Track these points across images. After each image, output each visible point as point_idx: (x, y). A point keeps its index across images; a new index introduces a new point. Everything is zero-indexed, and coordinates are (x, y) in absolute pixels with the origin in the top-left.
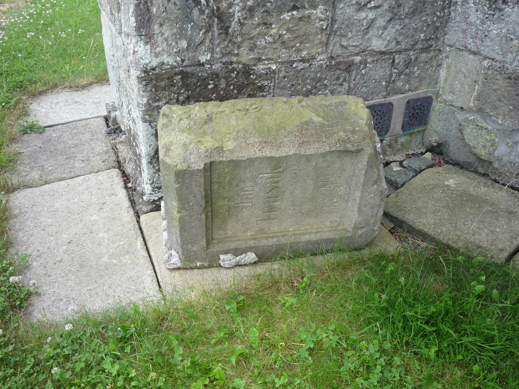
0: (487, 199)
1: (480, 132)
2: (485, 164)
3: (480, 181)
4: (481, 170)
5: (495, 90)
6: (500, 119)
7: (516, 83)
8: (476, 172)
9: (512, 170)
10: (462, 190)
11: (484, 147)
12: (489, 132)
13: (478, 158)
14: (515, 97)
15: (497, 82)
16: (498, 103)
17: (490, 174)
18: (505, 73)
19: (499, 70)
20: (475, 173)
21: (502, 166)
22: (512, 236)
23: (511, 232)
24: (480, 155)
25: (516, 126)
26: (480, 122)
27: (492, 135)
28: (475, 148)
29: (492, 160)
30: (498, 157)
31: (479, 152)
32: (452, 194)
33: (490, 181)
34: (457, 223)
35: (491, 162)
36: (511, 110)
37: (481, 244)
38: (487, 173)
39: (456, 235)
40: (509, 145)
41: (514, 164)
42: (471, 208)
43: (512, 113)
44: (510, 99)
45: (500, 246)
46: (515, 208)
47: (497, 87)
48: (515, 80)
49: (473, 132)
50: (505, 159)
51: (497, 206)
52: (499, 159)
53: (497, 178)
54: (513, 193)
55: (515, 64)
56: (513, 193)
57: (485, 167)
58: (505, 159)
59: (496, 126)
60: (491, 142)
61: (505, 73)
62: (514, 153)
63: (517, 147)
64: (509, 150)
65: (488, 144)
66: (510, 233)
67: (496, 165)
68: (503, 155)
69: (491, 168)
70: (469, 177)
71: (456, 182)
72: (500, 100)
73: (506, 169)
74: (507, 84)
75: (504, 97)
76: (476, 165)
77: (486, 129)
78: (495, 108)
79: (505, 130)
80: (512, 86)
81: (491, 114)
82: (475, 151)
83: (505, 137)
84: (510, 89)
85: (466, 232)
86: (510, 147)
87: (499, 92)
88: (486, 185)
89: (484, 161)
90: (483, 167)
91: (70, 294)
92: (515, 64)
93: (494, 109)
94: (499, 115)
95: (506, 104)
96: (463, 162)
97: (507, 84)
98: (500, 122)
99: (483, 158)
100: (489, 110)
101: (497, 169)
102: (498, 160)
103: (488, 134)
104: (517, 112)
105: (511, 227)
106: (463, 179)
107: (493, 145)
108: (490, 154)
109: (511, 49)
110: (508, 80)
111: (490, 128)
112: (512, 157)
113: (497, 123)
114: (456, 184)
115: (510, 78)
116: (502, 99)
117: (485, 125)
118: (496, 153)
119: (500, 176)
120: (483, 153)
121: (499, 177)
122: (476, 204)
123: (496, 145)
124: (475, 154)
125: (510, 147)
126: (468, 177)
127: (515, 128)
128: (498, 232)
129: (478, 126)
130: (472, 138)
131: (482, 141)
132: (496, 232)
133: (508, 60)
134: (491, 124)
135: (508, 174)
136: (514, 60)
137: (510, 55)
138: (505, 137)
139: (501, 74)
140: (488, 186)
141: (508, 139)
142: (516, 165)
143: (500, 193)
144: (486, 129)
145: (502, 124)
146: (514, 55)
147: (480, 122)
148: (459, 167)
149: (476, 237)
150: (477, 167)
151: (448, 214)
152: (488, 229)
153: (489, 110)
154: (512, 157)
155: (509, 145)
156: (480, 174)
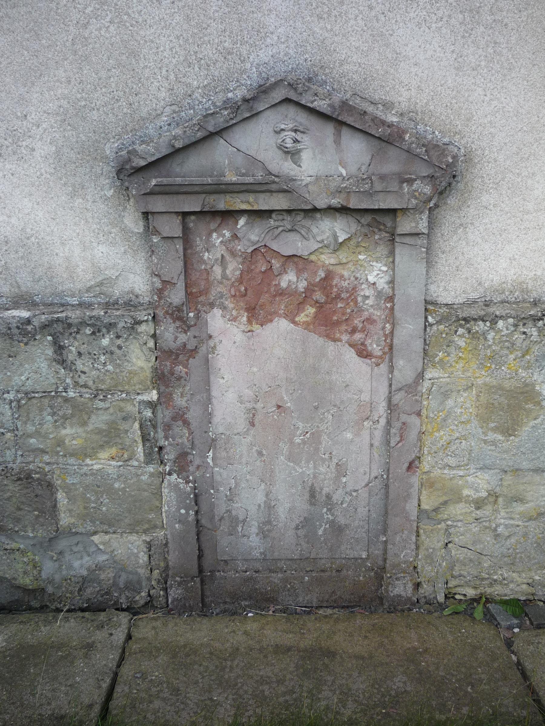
0: (53, 642)
1: (12, 556)
2: (38, 594)
3: (37, 620)
4: (35, 604)
5: (8, 499)
6: (30, 531)
7: (30, 483)
8: (30, 609)
9: (70, 588)
10: (17, 645)
11: (25, 573)
12: (23, 552)
13: (25, 590)
14: (36, 499)
15: (7, 488)
16: (19, 513)
17: (48, 604)
18: (12, 475)
19: (3, 473)
20: (30, 610)
21: (57, 587)
22: (98, 678)
23: (95, 673)
24: (26, 585)
25: (51, 534)
26: (8, 544)
27: (29, 554)
28: (14, 579)
29: (43, 585)
30: (48, 578)
31: (21, 581)
32: (5, 657)
33: (51, 614)
34: (22, 698)
35: (43, 589)
36: (37, 517)
37: (63, 712)
38: (44, 604)
39: (26, 717)
40: (54, 558)
41: (70, 579)
42: (35, 665)
43: (41, 520)
44: (31, 503)
45: (87, 701)
46: (90, 637)
47: (9, 494)
48: (27, 479)
49: (4, 559)
50: (57, 577)
51: (68, 646)
52: (51, 581)
53: (59, 606)
54: (83, 617)
55: (18, 461)
56: (83, 617)
57: (39, 598)
58: (57, 577)
59: (28, 542)
60: (31, 564)
61: (12, 475)
62: (64, 567)
63: (64, 557)
64: (57, 564)
65: (29, 568)
66: (95, 674)
67: (50, 589)
68: (53, 574)
69: (46, 597)
70: (21, 622)
71: (6, 637)
72: (19, 509)
73: (64, 589)
74: (20, 488)
75: (23, 503)
76: (26, 600)
77: (18, 550)
78: (18, 520)
79: (41, 544)
80: (27, 488)
81: (17, 529)
82: (17, 582)
83: (45, 551)
84: (25, 491)
85: (38, 705)
86: (56, 561)
87: (14, 500)
88: (47, 622)
89: (34, 591)
90: (35, 599)
91: (135, 9)
92: (18, 461)
93: (17, 522)
94: (26, 526)
95: (29, 511)
96: (8, 603)
97: (20, 488)
98: (31, 535)
99: (31, 587)
100: (11, 525)
101: (53, 594)
102: (50, 582)
103: (23, 555)
104: (45, 516)
105: (93, 666)
106: (14, 627)
107: (35, 567)
108: (37, 580)
109: (7, 445)
110: (19, 482)
111: (22, 546)
112: (64, 572)
113: (28, 537)
114: (6, 641)
115: (19, 479)
116: (22, 507)
117: (14, 545)
118: (44, 575)
119: (61, 601)
120: (27, 581)
121: (60, 603)
122: (40, 657)
123: (39, 564)
124: (19, 587)
125: (56, 561)
126: (20, 622)
127: (52, 536)
128: (79, 683)
129: (6, 550)
130: (6, 568)
131: (19, 567)
132: (77, 683)
133: (9, 459)
134: (21, 541)
135: (68, 595)
136: (16, 457)
137: (8, 452)
138: (45, 551)
139: (7, 477)
140: (50, 622)
141: (50, 553)
142: (73, 580)
143: (67, 625)
144: (18, 550)
145: (34, 537)
146: (13, 450)
147: (8, 544)
148: (6, 611)
149: (53, 704)
150: (29, 602)
151: (6, 691)
152: (66, 686)
153: (11, 525)
154: (64, 572)
155: (54, 558)
156: (36, 609)
